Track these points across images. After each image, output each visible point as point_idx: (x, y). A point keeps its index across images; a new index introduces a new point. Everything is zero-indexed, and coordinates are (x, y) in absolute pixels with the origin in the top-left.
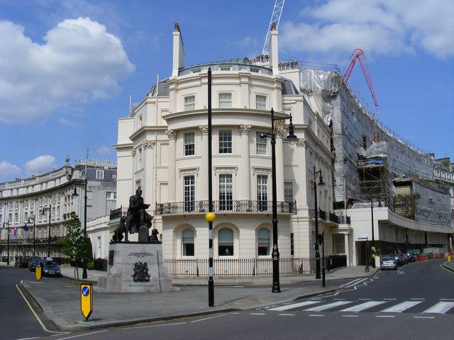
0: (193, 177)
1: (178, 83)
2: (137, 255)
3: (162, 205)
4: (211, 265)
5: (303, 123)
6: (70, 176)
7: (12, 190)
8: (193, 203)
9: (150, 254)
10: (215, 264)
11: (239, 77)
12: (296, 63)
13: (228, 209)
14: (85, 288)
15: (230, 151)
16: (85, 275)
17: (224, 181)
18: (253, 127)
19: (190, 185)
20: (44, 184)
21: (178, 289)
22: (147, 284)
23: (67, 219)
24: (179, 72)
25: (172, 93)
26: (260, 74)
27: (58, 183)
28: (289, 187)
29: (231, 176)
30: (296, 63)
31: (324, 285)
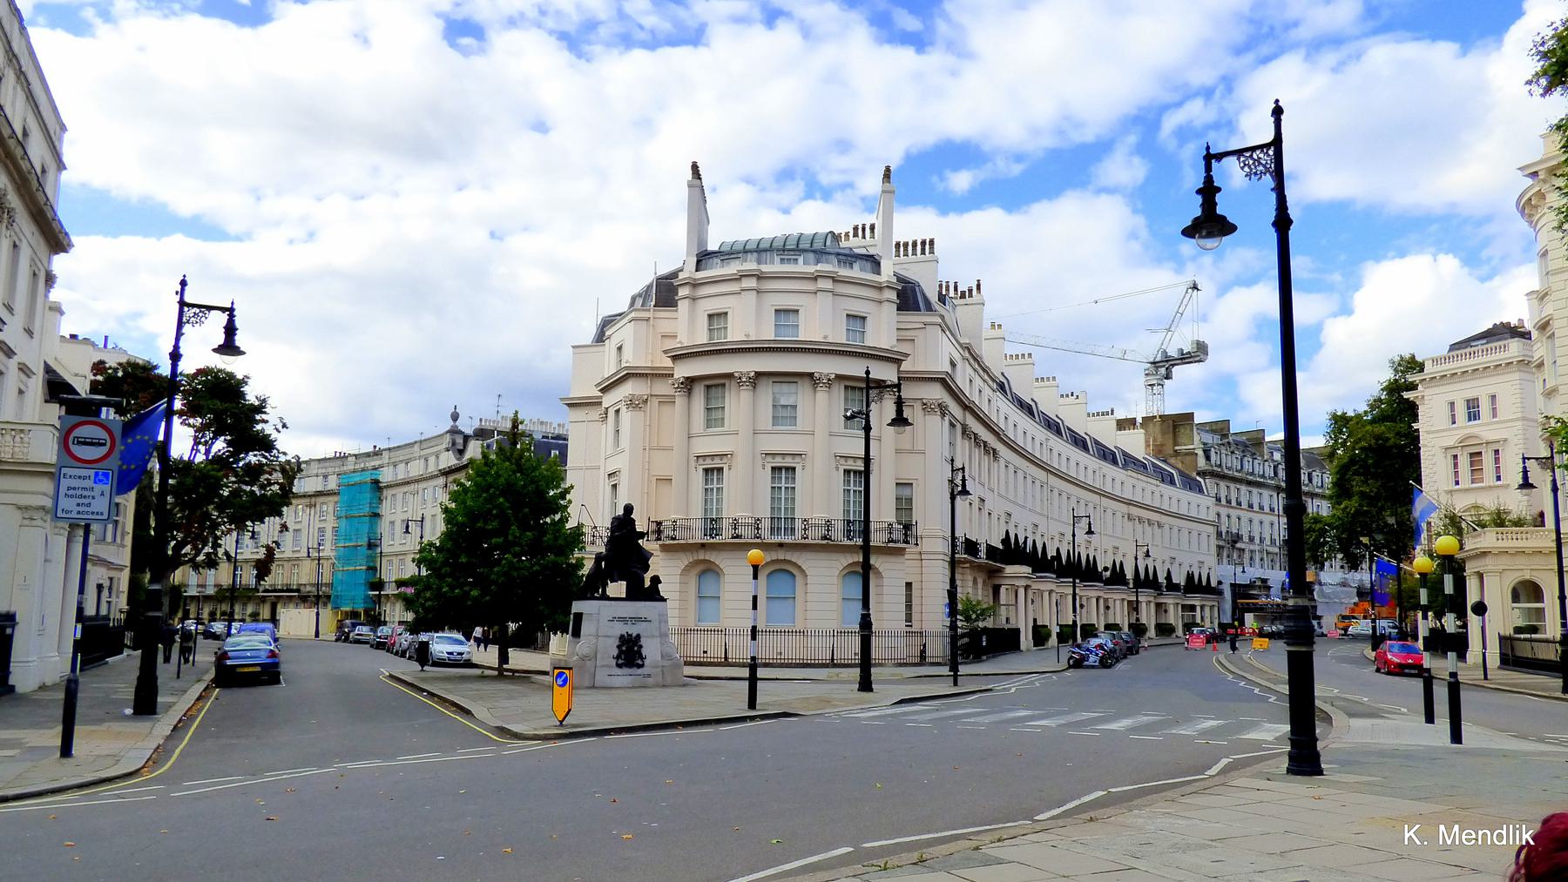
0: (720, 470)
1: (695, 285)
2: (623, 620)
3: (659, 524)
4: (754, 629)
7: (325, 477)
9: (646, 620)
10: (759, 637)
14: (560, 675)
16: (504, 658)
19: (715, 486)
20: (401, 467)
22: (640, 671)
24: (698, 262)
25: (683, 306)
28: (906, 492)
31: (956, 684)
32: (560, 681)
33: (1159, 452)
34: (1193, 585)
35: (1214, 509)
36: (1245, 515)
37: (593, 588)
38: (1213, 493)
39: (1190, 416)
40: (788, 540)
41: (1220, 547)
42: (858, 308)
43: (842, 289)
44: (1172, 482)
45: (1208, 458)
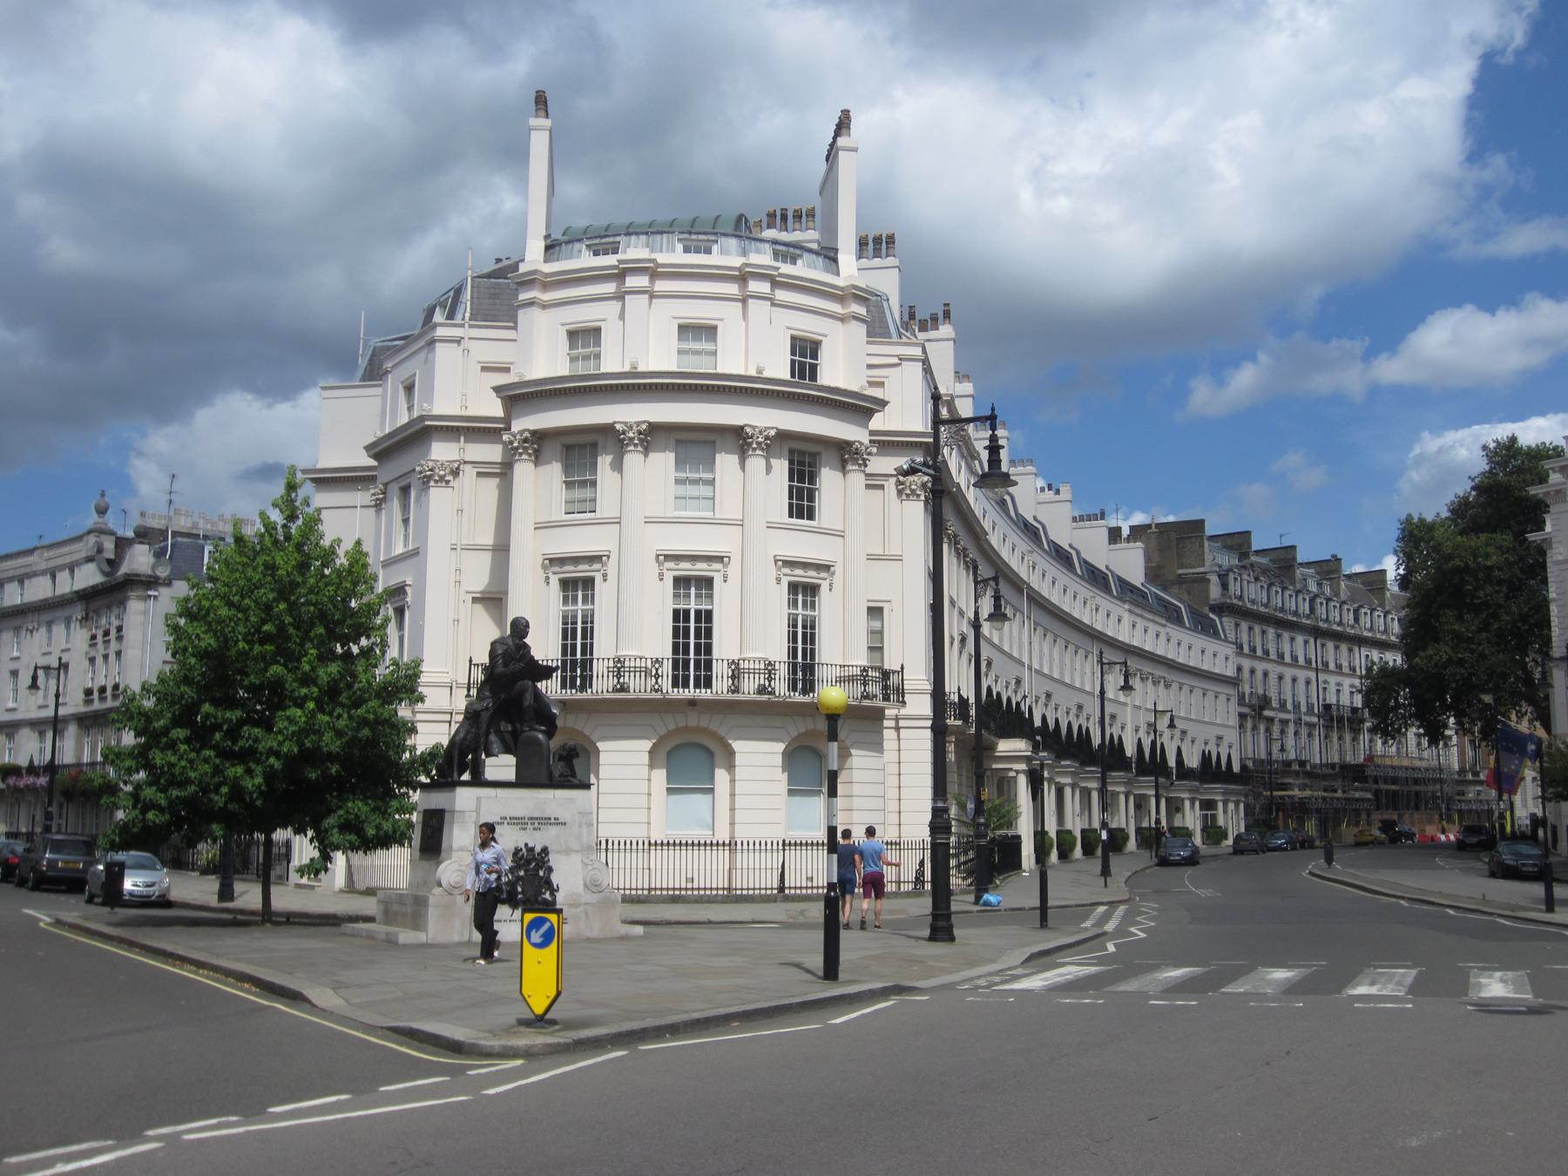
0: (589, 583)
5: (920, 428)
6: (113, 564)
8: (587, 664)
9: (558, 822)
13: (697, 685)
15: (811, 517)
17: (575, 601)
18: (783, 436)
20: (63, 576)
21: (639, 930)
23: (97, 705)
24: (548, 248)
27: (66, 585)
32: (536, 937)
33: (1153, 574)
34: (1211, 771)
35: (1234, 661)
36: (1274, 670)
37: (457, 764)
38: (1232, 637)
39: (1199, 525)
40: (704, 694)
41: (1242, 716)
42: (809, 325)
44: (1178, 620)
45: (1225, 586)
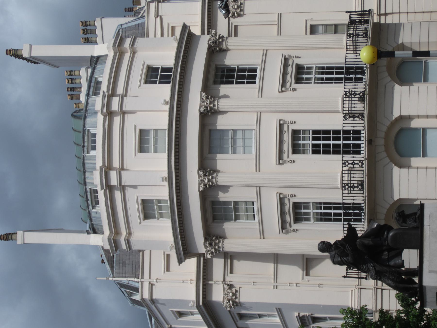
0: (297, 206)
8: (346, 206)
11: (109, 114)
12: (85, 23)
13: (359, 139)
17: (308, 214)
18: (206, 88)
26: (104, 80)
29: (296, 133)
30: (85, 23)
40: (364, 135)
42: (138, 73)
43: (120, 90)
